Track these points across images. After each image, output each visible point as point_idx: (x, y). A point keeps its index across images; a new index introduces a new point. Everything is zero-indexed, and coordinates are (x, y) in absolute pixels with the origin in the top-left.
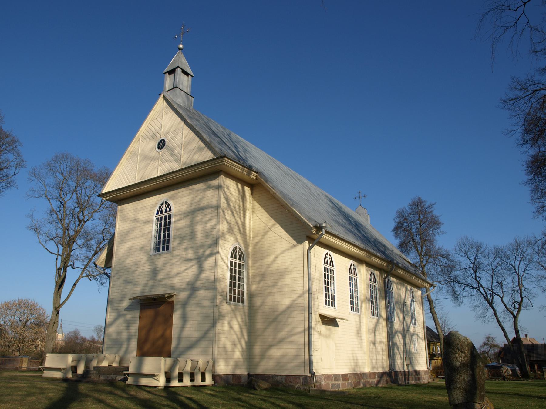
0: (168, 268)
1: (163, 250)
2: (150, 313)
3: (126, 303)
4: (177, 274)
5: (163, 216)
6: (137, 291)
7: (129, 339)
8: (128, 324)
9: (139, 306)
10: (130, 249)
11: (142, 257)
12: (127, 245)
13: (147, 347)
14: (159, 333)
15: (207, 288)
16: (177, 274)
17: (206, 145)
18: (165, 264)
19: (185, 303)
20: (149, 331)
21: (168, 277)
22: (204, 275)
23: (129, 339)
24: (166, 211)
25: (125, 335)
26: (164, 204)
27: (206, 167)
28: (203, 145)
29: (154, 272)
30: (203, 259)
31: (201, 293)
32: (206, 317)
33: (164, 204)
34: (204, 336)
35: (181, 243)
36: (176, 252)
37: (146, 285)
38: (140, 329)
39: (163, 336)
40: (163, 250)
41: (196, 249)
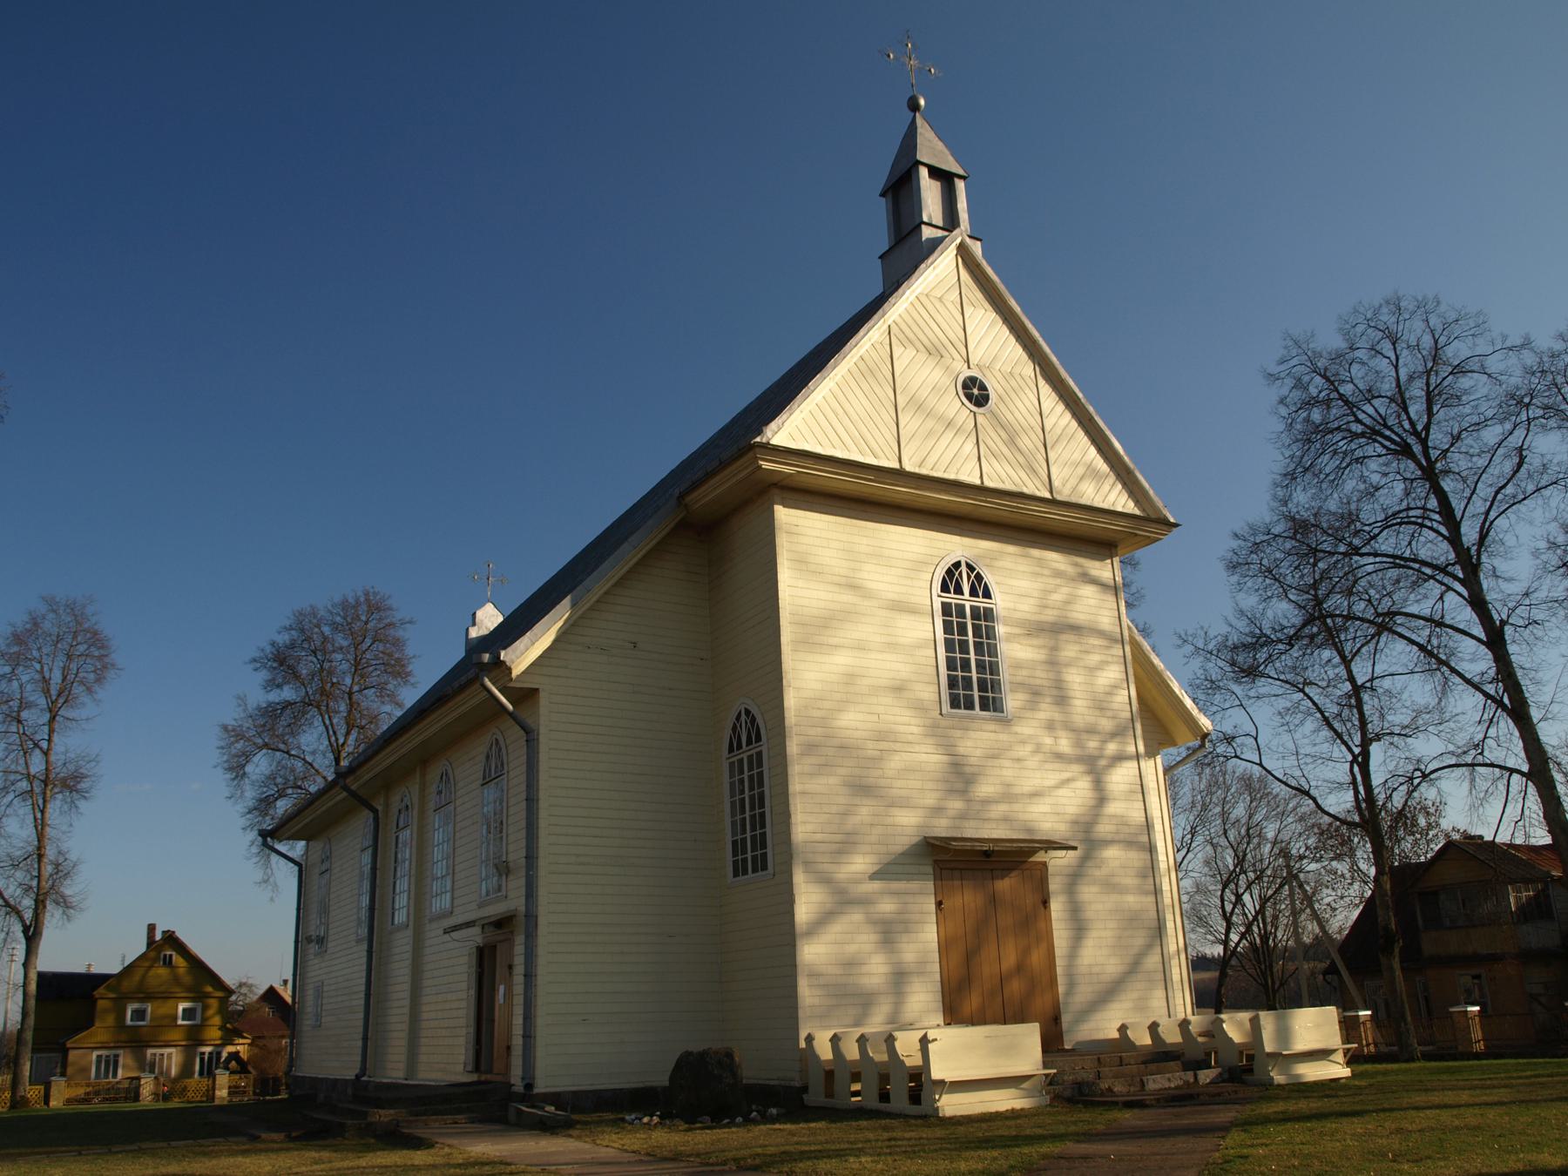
0: (1007, 771)
1: (755, 871)
2: (967, 898)
3: (860, 864)
4: (1036, 795)
5: (745, 756)
6: (908, 823)
7: (899, 979)
8: (889, 932)
9: (930, 869)
10: (850, 678)
11: (908, 724)
12: (841, 661)
13: (973, 1002)
14: (1010, 959)
15: (1130, 844)
16: (1036, 795)
17: (1112, 467)
18: (994, 755)
19: (1075, 877)
20: (970, 957)
21: (1008, 796)
22: (1113, 808)
23: (899, 979)
24: (749, 742)
25: (876, 970)
26: (743, 716)
27: (1102, 524)
28: (1101, 465)
29: (960, 776)
30: (1103, 762)
31: (1113, 854)
32: (1131, 920)
33: (743, 716)
34: (1134, 968)
35: (1032, 705)
36: (1025, 729)
37: (938, 810)
38: (945, 947)
39: (1020, 968)
40: (755, 871)
41: (1080, 733)
